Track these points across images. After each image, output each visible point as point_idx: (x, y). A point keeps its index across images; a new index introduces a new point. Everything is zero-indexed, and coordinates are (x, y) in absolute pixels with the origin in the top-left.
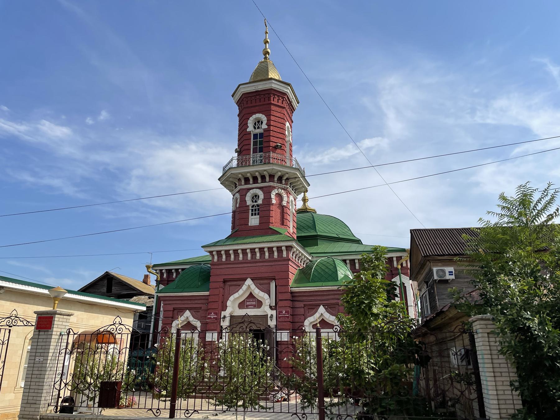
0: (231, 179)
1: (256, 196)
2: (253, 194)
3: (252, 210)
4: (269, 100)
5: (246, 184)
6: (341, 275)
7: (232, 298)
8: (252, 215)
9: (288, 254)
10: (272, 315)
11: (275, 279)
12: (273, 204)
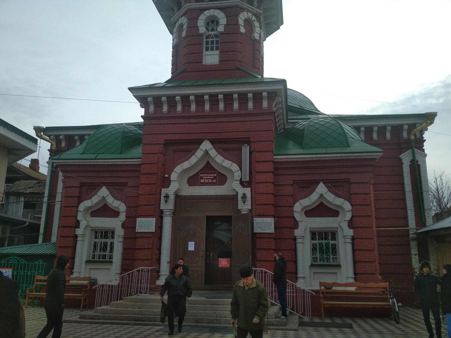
1: (213, 22)
7: (179, 169)
8: (207, 49)
9: (270, 104)
10: (244, 194)
11: (249, 142)
12: (241, 34)
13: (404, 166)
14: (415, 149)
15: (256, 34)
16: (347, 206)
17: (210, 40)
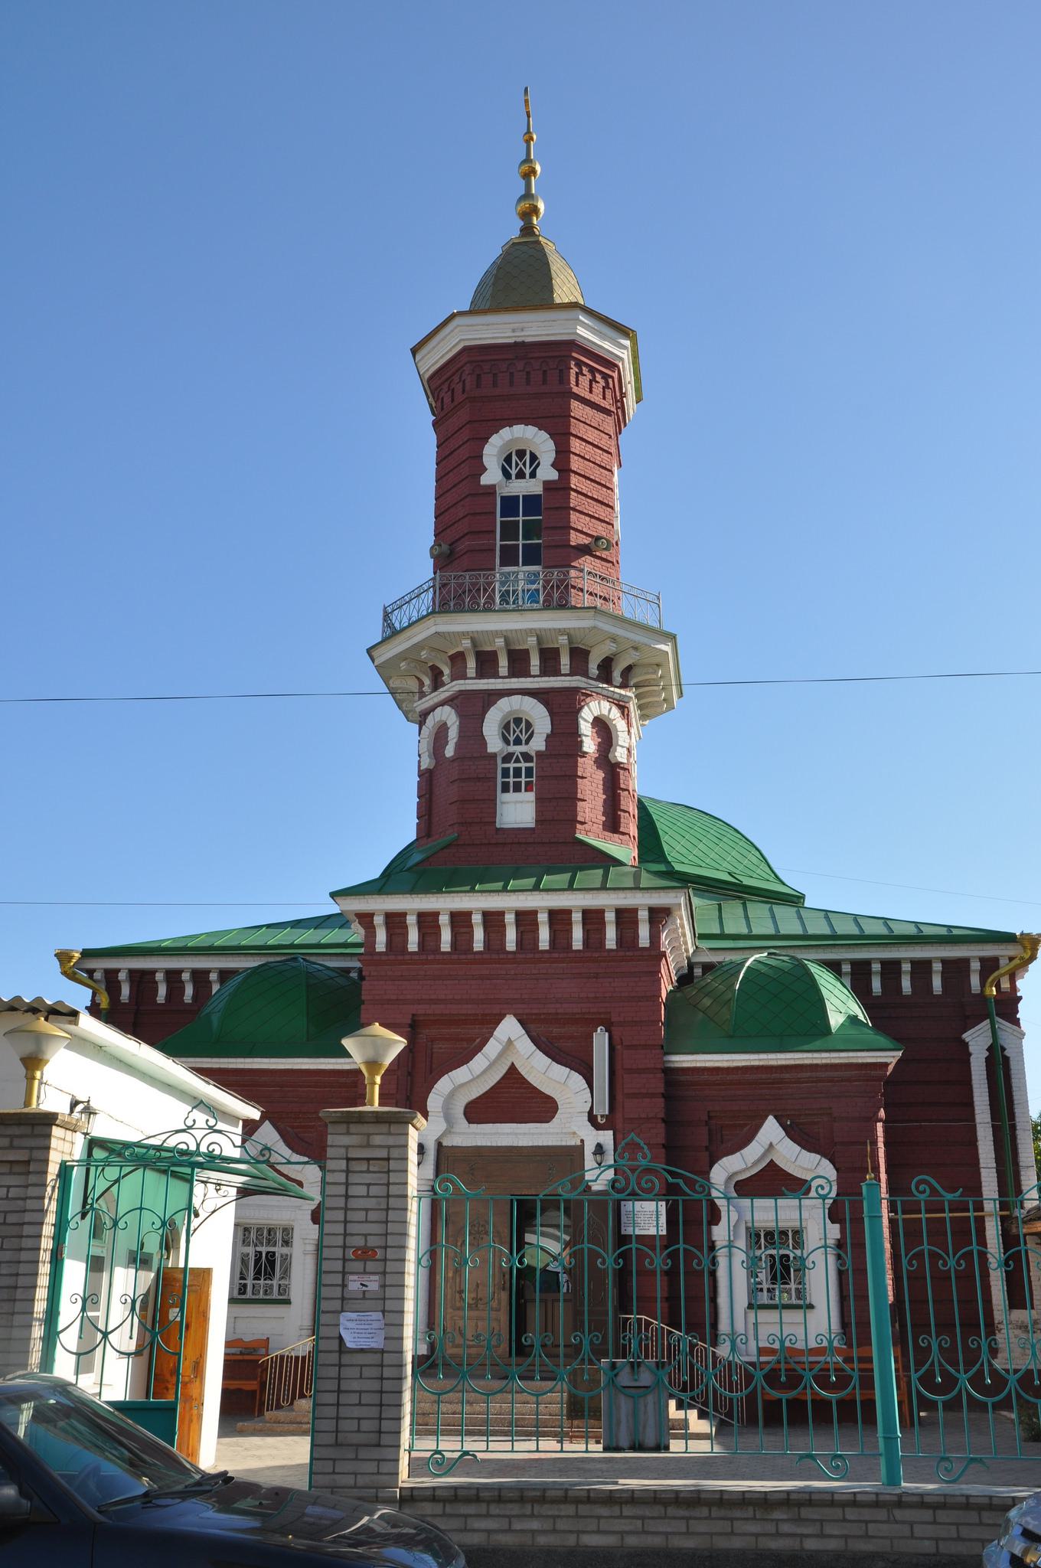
0: (424, 654)
2: (510, 713)
3: (506, 773)
4: (563, 378)
5: (481, 674)
6: (836, 1020)
7: (444, 1085)
8: (505, 788)
12: (584, 755)
13: (972, 1059)
14: (997, 1019)
15: (619, 749)
16: (828, 1170)
17: (512, 765)
